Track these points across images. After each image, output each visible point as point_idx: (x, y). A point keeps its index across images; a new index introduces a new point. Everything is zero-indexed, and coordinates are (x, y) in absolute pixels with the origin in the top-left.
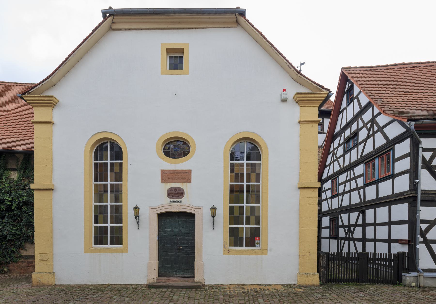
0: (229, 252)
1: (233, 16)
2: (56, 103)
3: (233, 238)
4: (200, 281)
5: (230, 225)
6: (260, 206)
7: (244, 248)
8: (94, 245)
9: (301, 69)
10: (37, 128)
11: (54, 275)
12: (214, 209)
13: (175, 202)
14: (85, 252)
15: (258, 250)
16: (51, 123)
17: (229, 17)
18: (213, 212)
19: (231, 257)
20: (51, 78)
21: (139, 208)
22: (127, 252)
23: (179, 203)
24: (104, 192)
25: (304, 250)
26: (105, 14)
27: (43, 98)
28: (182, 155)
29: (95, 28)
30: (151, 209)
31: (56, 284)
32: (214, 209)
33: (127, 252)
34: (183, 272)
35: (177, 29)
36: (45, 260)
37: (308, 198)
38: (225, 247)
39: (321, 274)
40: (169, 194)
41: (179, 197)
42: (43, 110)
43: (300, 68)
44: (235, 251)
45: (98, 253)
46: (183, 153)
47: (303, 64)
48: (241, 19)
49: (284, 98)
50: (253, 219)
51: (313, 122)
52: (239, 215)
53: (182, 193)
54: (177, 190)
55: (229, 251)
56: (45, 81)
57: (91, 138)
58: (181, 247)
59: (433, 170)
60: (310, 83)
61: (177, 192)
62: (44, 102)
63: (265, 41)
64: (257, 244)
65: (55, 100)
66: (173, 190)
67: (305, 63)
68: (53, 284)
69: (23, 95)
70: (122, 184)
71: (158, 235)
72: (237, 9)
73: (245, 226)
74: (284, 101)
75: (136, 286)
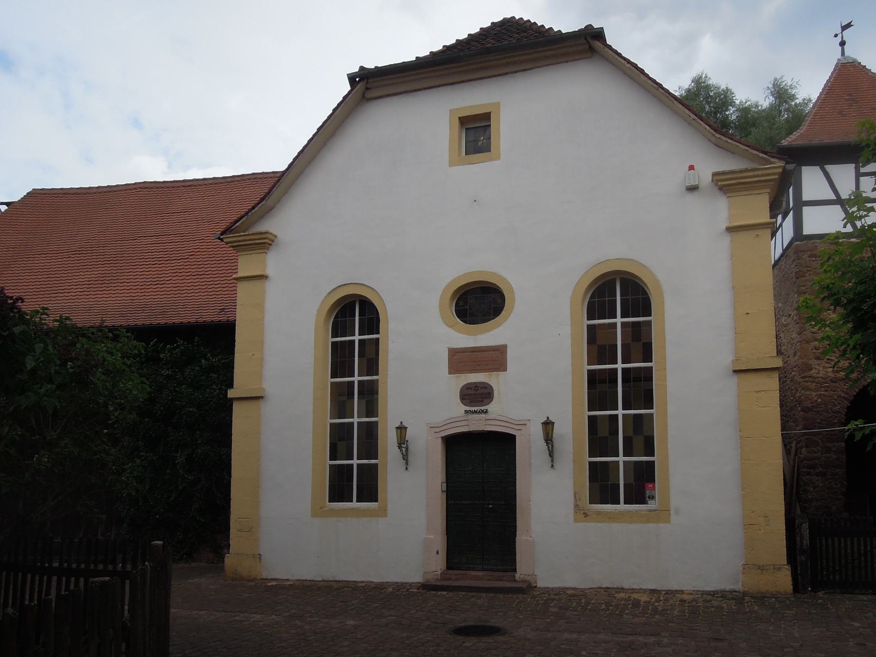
0: (585, 517)
2: (273, 241)
4: (528, 578)
6: (654, 415)
7: (622, 507)
9: (844, 39)
10: (242, 288)
12: (548, 425)
13: (475, 412)
14: (312, 516)
15: (650, 511)
16: (263, 277)
17: (573, 43)
19: (592, 527)
20: (267, 200)
22: (386, 516)
23: (483, 415)
24: (348, 395)
25: (753, 512)
26: (352, 78)
27: (251, 237)
28: (492, 315)
29: (336, 105)
32: (548, 425)
33: (386, 516)
34: (495, 559)
36: (247, 530)
37: (756, 392)
38: (576, 506)
39: (799, 569)
40: (464, 397)
41: (483, 401)
42: (252, 255)
43: (842, 38)
44: (599, 514)
45: (335, 518)
46: (492, 311)
47: (849, 25)
48: (597, 44)
49: (691, 184)
50: (638, 442)
52: (610, 435)
53: (490, 394)
54: (479, 388)
55: (586, 515)
56: (256, 206)
57: (326, 297)
58: (491, 506)
60: (742, 149)
61: (478, 392)
62: (253, 242)
63: (644, 79)
64: (649, 498)
65: (271, 237)
66: (471, 388)
67: (852, 24)
69: (222, 236)
70: (377, 380)
71: (445, 481)
72: (584, 32)
73: (621, 459)
74: (692, 189)
75: (402, 585)
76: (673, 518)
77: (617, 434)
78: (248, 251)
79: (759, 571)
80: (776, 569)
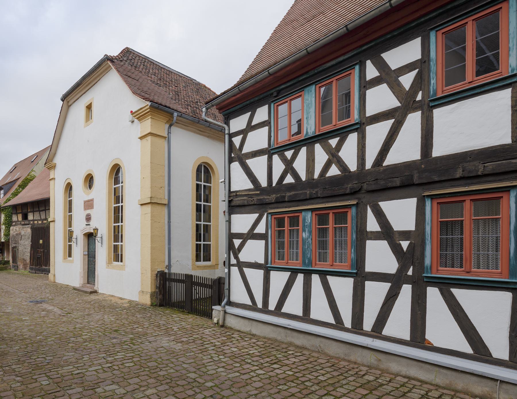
35: (90, 88)
59: (244, 161)
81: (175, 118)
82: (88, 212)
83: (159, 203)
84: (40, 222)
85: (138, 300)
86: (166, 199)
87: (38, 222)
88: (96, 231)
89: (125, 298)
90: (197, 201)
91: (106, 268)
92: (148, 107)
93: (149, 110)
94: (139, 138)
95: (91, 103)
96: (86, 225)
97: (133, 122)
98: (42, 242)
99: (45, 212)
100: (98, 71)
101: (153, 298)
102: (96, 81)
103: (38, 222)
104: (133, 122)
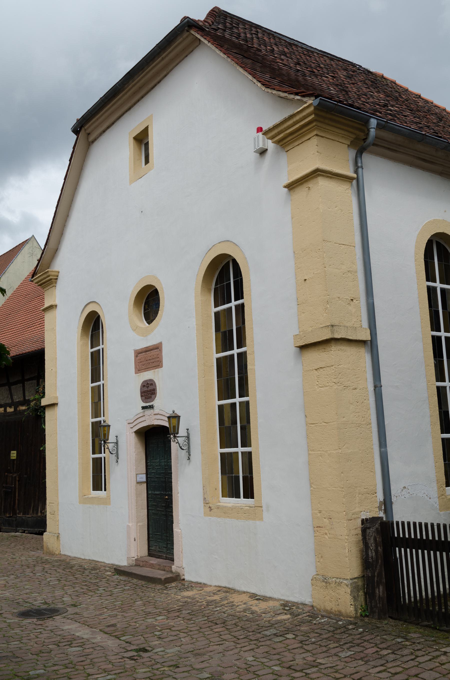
1: (186, 34)
2: (58, 276)
3: (226, 477)
5: (221, 448)
8: (93, 490)
11: (58, 538)
18: (174, 425)
21: (178, 417)
26: (76, 130)
30: (129, 423)
31: (61, 553)
37: (316, 370)
51: (308, 177)
68: (56, 552)
76: (265, 514)
77: (236, 424)
78: (47, 286)
79: (324, 584)
80: (337, 584)
81: (373, 132)
82: (147, 375)
83: (350, 338)
84: (10, 410)
85: (308, 600)
86: (366, 329)
87: (5, 410)
88: (174, 421)
89: (268, 594)
90: (432, 330)
91: (206, 514)
92: (312, 109)
93: (313, 116)
94: (285, 187)
95: (147, 128)
96: (143, 408)
97: (263, 152)
98: (15, 455)
99: (21, 385)
100: (164, 55)
101: (358, 595)
102: (158, 79)
103: (5, 410)
104: (263, 152)
